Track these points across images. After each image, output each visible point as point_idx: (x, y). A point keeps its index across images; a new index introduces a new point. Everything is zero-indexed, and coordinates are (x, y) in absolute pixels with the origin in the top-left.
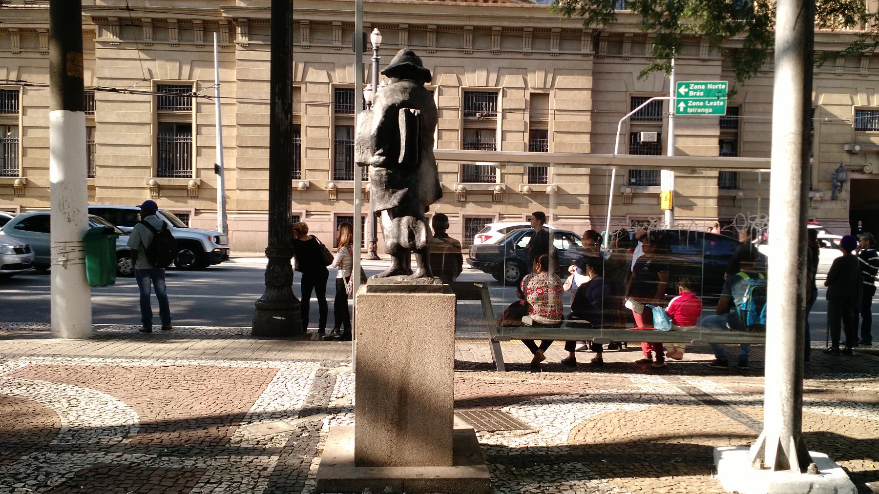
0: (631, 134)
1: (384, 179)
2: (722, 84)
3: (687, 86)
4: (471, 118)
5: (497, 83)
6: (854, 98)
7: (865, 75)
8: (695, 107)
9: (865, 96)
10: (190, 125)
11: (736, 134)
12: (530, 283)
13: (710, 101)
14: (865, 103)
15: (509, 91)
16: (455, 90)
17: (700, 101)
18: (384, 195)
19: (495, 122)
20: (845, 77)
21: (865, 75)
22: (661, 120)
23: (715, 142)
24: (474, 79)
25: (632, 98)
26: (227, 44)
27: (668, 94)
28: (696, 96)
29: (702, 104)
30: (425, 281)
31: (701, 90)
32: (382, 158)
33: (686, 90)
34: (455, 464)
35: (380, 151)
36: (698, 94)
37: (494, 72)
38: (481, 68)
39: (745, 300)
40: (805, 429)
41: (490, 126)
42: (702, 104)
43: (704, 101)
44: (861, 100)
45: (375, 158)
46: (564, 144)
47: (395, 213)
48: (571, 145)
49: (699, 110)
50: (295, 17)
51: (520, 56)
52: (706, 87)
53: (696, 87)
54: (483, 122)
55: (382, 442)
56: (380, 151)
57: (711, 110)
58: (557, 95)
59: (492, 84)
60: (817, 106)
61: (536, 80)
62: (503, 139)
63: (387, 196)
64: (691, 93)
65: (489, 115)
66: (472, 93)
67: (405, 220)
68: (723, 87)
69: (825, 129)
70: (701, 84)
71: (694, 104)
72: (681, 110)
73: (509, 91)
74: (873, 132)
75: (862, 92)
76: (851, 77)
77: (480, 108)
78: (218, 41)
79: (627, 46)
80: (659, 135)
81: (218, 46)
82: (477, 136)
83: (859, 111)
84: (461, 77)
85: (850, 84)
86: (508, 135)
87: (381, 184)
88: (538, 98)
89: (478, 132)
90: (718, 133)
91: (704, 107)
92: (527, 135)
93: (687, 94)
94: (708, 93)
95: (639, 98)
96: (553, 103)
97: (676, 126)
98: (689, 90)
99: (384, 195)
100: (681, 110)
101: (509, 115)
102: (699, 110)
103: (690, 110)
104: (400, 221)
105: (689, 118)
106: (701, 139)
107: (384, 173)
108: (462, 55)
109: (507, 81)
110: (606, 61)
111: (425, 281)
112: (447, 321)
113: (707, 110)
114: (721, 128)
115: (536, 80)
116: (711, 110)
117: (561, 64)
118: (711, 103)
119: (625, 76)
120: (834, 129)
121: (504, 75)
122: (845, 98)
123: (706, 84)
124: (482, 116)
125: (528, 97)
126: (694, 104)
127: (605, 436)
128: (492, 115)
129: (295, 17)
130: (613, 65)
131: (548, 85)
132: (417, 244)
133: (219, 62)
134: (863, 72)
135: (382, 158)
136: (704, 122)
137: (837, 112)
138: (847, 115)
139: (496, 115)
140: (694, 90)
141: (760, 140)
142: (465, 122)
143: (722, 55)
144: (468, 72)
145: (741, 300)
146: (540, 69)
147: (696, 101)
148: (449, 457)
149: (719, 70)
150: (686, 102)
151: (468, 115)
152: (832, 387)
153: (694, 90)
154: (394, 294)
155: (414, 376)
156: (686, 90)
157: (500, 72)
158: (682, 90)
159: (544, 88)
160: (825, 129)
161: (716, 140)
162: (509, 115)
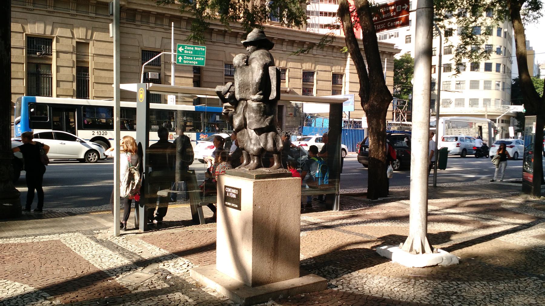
1: (262, 110)
2: (203, 48)
3: (183, 47)
4: (33, 56)
5: (52, 32)
8: (188, 60)
10: (50, 65)
11: (200, 77)
12: (218, 168)
13: (196, 57)
15: (61, 39)
16: (20, 35)
18: (260, 120)
19: (51, 59)
22: (160, 66)
23: (191, 81)
24: (35, 28)
25: (142, 51)
26: (168, 27)
27: (170, 50)
28: (188, 54)
29: (192, 58)
30: (281, 170)
31: (191, 50)
32: (262, 97)
33: (183, 49)
34: (301, 275)
35: (261, 92)
36: (190, 52)
37: (49, 25)
38: (40, 21)
39: (318, 172)
40: (429, 232)
41: (47, 62)
42: (192, 58)
43: (193, 57)
45: (256, 97)
46: (101, 77)
47: (259, 131)
48: (105, 78)
49: (190, 62)
51: (68, 16)
53: (188, 48)
54: (42, 58)
55: (267, 269)
56: (261, 92)
57: (197, 63)
58: (95, 45)
59: (48, 33)
61: (80, 33)
62: (57, 71)
63: (262, 120)
64: (186, 52)
65: (47, 54)
66: (33, 38)
67: (270, 134)
68: (204, 49)
70: (191, 47)
72: (180, 61)
73: (61, 39)
75: (285, 60)
77: (40, 50)
79: (152, 19)
80: (159, 75)
82: (37, 68)
84: (25, 26)
86: (61, 69)
87: (260, 111)
88: (81, 46)
89: (38, 66)
90: (193, 76)
91: (193, 60)
92: (74, 70)
93: (183, 52)
94: (195, 52)
95: (154, 52)
96: (91, 50)
97: (176, 71)
98: (185, 50)
99: (260, 120)
100: (180, 61)
101: (61, 55)
102: (190, 62)
104: (267, 135)
105: (183, 66)
106: (183, 79)
107: (262, 105)
108: (25, 11)
109: (59, 32)
110: (125, 25)
111: (281, 170)
112: (297, 193)
113: (194, 63)
114: (194, 73)
115: (80, 33)
116: (197, 63)
117: (97, 24)
119: (137, 36)
121: (57, 28)
123: (194, 47)
124: (41, 54)
125: (75, 44)
128: (49, 55)
130: (130, 28)
131: (89, 38)
132: (278, 148)
134: (284, 49)
135: (262, 97)
136: (185, 68)
139: (52, 55)
140: (187, 50)
141: (212, 81)
142: (28, 58)
143: (193, 30)
144: (29, 23)
145: (315, 171)
146: (83, 27)
148: (298, 272)
150: (183, 57)
151: (31, 53)
152: (362, 213)
153: (187, 50)
154: (274, 179)
155: (282, 228)
156: (183, 49)
157: (54, 25)
158: (181, 49)
159: (86, 39)
161: (191, 80)
162: (61, 55)
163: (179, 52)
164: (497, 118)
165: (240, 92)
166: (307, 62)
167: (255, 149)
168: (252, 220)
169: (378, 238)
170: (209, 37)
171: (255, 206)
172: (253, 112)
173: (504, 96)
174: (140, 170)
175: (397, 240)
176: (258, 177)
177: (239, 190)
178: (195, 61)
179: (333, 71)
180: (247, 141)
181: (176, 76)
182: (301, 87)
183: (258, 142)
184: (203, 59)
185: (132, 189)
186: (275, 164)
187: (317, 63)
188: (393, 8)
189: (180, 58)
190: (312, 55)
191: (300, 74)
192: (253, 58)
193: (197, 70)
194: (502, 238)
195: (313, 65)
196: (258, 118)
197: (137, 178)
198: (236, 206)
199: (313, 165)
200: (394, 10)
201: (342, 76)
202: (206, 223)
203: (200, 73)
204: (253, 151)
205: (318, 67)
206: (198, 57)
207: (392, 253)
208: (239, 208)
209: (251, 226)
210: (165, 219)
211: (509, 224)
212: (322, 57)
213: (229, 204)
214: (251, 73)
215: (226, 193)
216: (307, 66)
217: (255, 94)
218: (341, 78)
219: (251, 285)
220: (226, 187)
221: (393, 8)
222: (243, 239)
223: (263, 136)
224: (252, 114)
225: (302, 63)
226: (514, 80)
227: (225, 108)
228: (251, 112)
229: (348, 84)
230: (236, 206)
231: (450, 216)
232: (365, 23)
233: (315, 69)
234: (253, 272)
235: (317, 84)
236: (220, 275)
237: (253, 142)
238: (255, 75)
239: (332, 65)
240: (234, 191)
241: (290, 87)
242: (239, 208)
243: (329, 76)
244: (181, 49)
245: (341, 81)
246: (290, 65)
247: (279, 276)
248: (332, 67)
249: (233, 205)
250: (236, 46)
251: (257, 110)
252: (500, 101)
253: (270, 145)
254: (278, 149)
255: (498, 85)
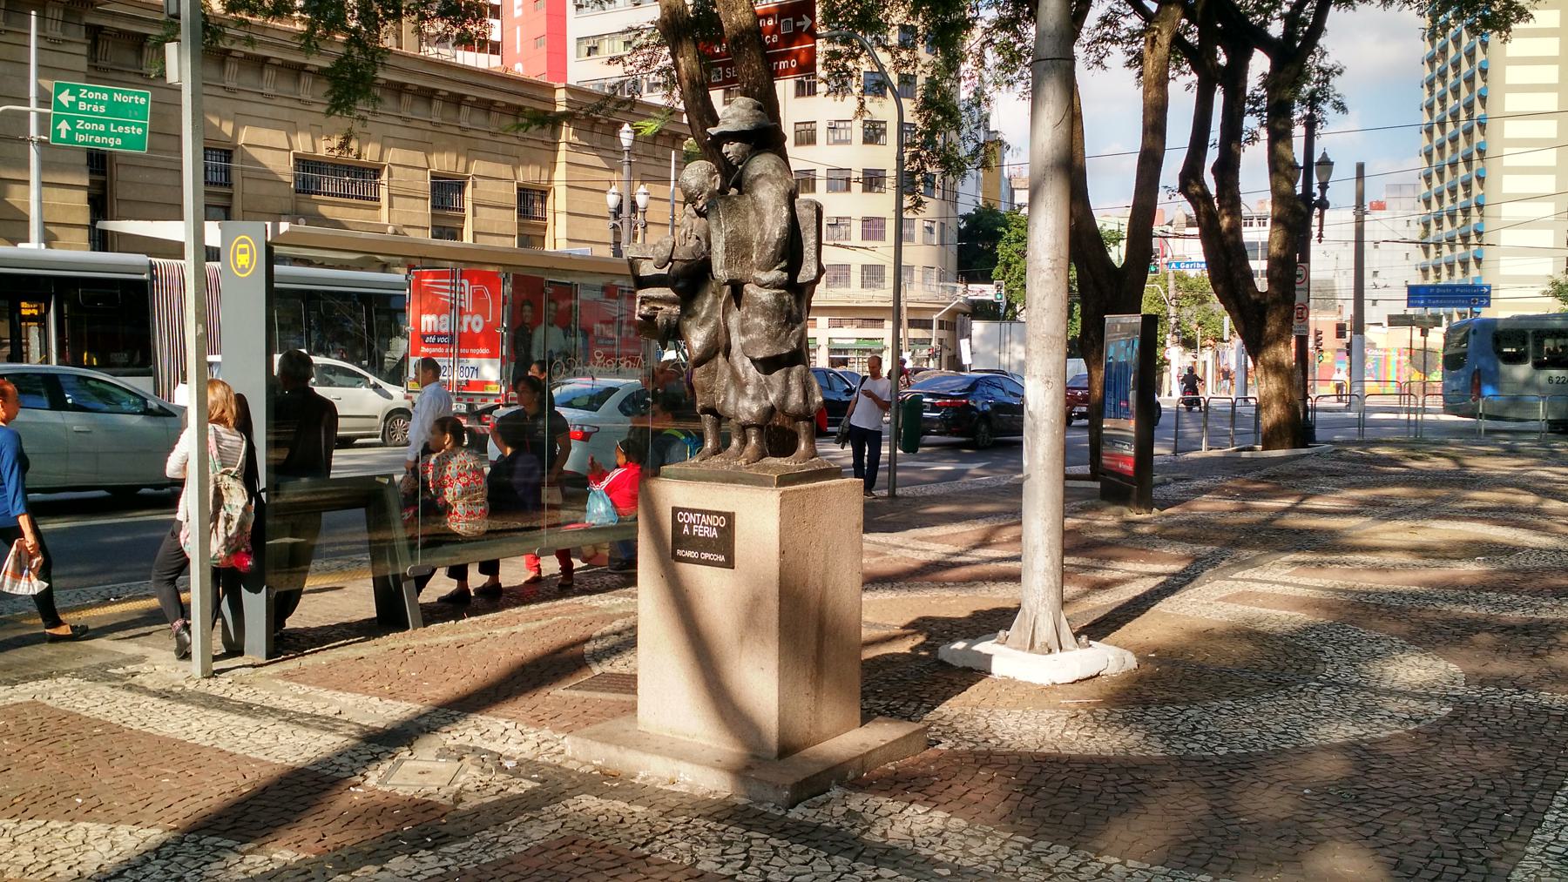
0: (1390, 324)
2: (140, 95)
6: (293, 139)
7: (269, 96)
8: (90, 132)
9: (309, 137)
11: (104, 184)
13: (117, 124)
14: (310, 149)
17: (99, 122)
20: (277, 101)
21: (269, 96)
27: (26, 102)
29: (102, 128)
31: (101, 102)
33: (73, 99)
34: (866, 718)
35: (784, 264)
36: (95, 109)
42: (102, 128)
43: (107, 123)
44: (302, 144)
45: (774, 275)
49: (98, 139)
50: (1196, 231)
52: (111, 97)
53: (91, 95)
56: (784, 264)
57: (119, 142)
60: (237, 147)
64: (82, 106)
68: (143, 100)
69: (250, 188)
70: (102, 91)
71: (88, 126)
72: (63, 135)
74: (322, 197)
75: (303, 130)
76: (286, 103)
78: (39, 28)
81: (39, 37)
83: (303, 163)
85: (285, 114)
90: (86, 183)
91: (107, 133)
93: (74, 105)
94: (114, 108)
97: (44, 166)
100: (63, 135)
102: (98, 139)
103: (80, 138)
104: (788, 373)
106: (55, 190)
113: (111, 141)
114: (91, 172)
118: (120, 129)
120: (265, 189)
122: (278, 138)
126: (88, 126)
127: (306, 754)
129: (1196, 231)
133: (39, 66)
134: (435, 120)
137: (270, 160)
138: (283, 166)
140: (88, 101)
147: (91, 121)
149: (82, 64)
150: (72, 122)
153: (88, 101)
156: (73, 99)
158: (65, 98)
160: (250, 188)
161: (84, 194)
163: (59, 106)
164: (935, 317)
165: (728, 264)
166: (442, 150)
167: (755, 409)
168: (776, 591)
169: (903, 628)
170: (130, 58)
171: (782, 553)
172: (763, 314)
173: (943, 259)
174: (248, 475)
175: (996, 621)
176: (784, 480)
177: (730, 517)
178: (112, 135)
179: (521, 180)
180: (726, 391)
181: (44, 184)
182: (428, 222)
183: (762, 390)
184: (139, 131)
185: (227, 539)
186: (803, 446)
187: (472, 153)
188: (770, 23)
189: (64, 126)
190: (457, 131)
191: (424, 183)
192: (760, 176)
193: (98, 161)
194: (1164, 606)
195: (462, 161)
196: (773, 330)
197: (237, 499)
198: (722, 558)
199: (676, 448)
200: (776, 29)
201: (544, 194)
202: (425, 626)
203: (104, 173)
204: (751, 413)
205: (477, 167)
206: (125, 124)
207: (990, 656)
208: (729, 563)
209: (772, 604)
210: (291, 623)
211: (1142, 575)
212: (487, 136)
213: (689, 554)
214: (752, 213)
215: (677, 527)
216: (444, 162)
217: (768, 269)
218: (544, 201)
219: (775, 754)
220: (675, 510)
221: (770, 23)
222: (742, 639)
223: (778, 375)
224: (760, 321)
225: (428, 153)
226: (965, 217)
227: (642, 303)
228: (756, 313)
229: (562, 219)
230: (722, 558)
231: (1002, 565)
232: (749, 66)
233: (467, 171)
234: (781, 720)
235: (474, 214)
236: (666, 736)
237: (750, 390)
238: (769, 219)
239: (517, 161)
240: (710, 520)
241: (396, 220)
242: (729, 563)
243: (510, 194)
244: (65, 98)
245: (544, 210)
246: (393, 155)
247: (826, 727)
248: (515, 167)
249: (706, 556)
250: (221, 92)
251: (774, 309)
252: (935, 274)
253: (795, 399)
254: (813, 407)
255: (930, 230)
